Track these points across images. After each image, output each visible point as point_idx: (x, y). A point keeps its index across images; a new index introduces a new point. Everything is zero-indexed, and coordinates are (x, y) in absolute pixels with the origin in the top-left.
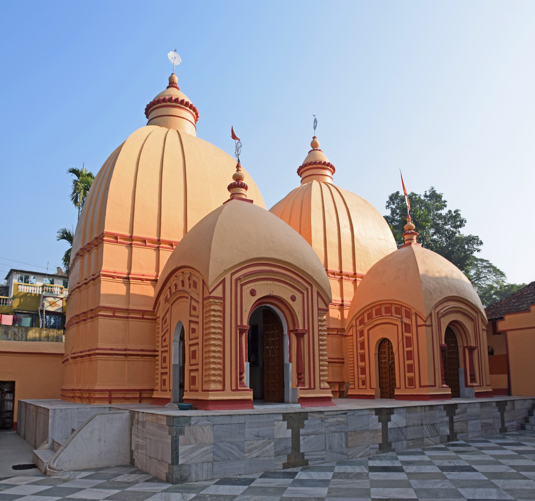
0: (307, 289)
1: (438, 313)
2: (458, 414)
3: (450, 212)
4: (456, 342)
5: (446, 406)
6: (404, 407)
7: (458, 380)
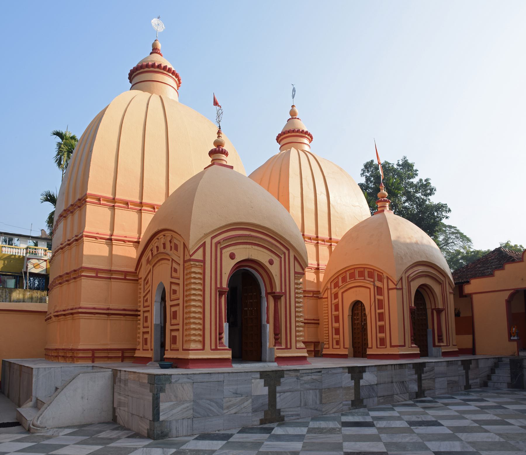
0: (285, 254)
1: (408, 277)
3: (421, 180)
5: (415, 365)
6: (375, 366)
7: (427, 340)
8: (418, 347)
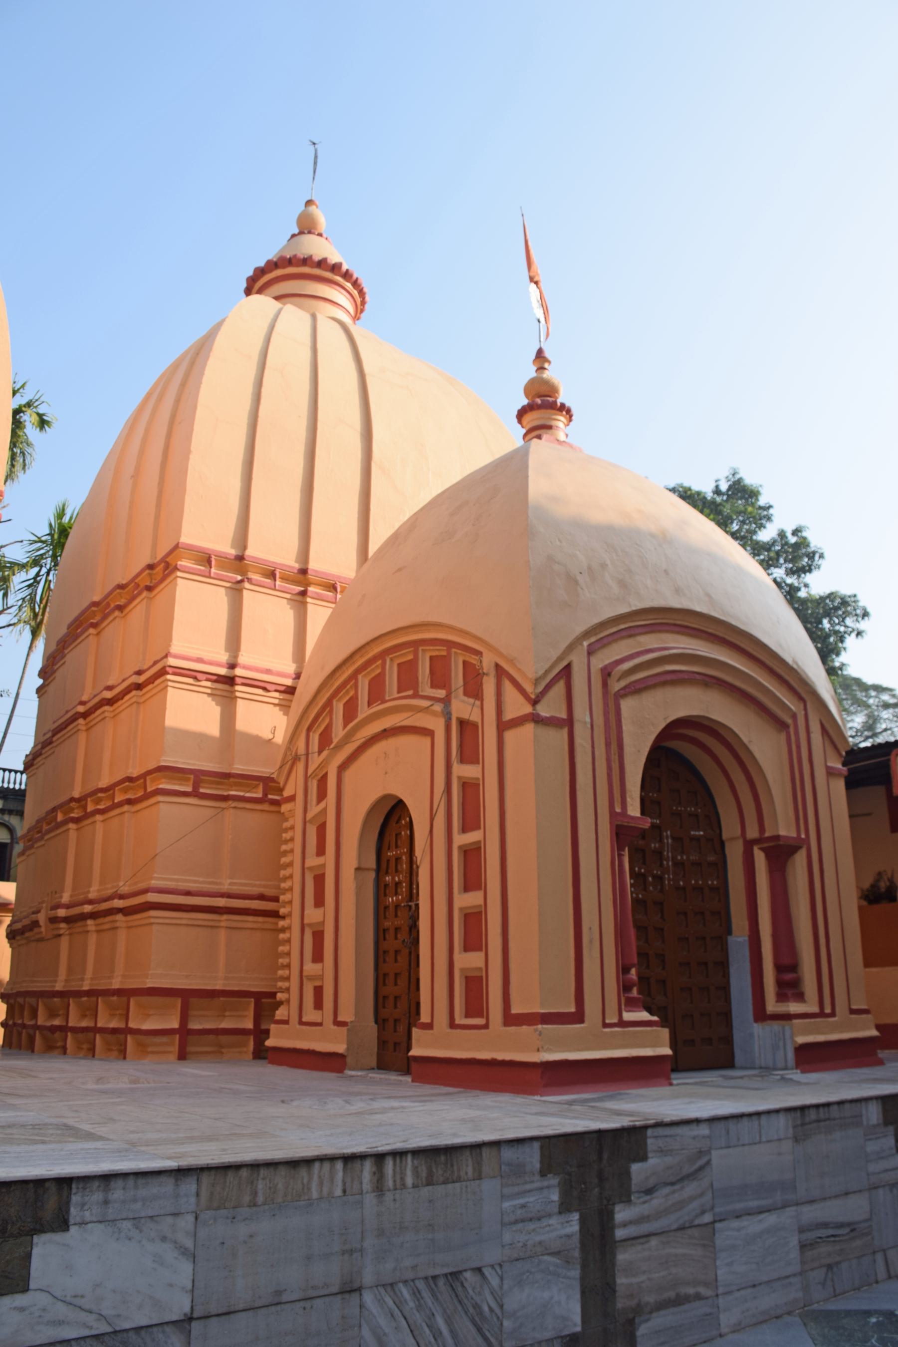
1: (606, 673)
2: (649, 1191)
3: (782, 534)
4: (714, 820)
5: (557, 1150)
6: (181, 1172)
7: (725, 989)
8: (663, 1023)
